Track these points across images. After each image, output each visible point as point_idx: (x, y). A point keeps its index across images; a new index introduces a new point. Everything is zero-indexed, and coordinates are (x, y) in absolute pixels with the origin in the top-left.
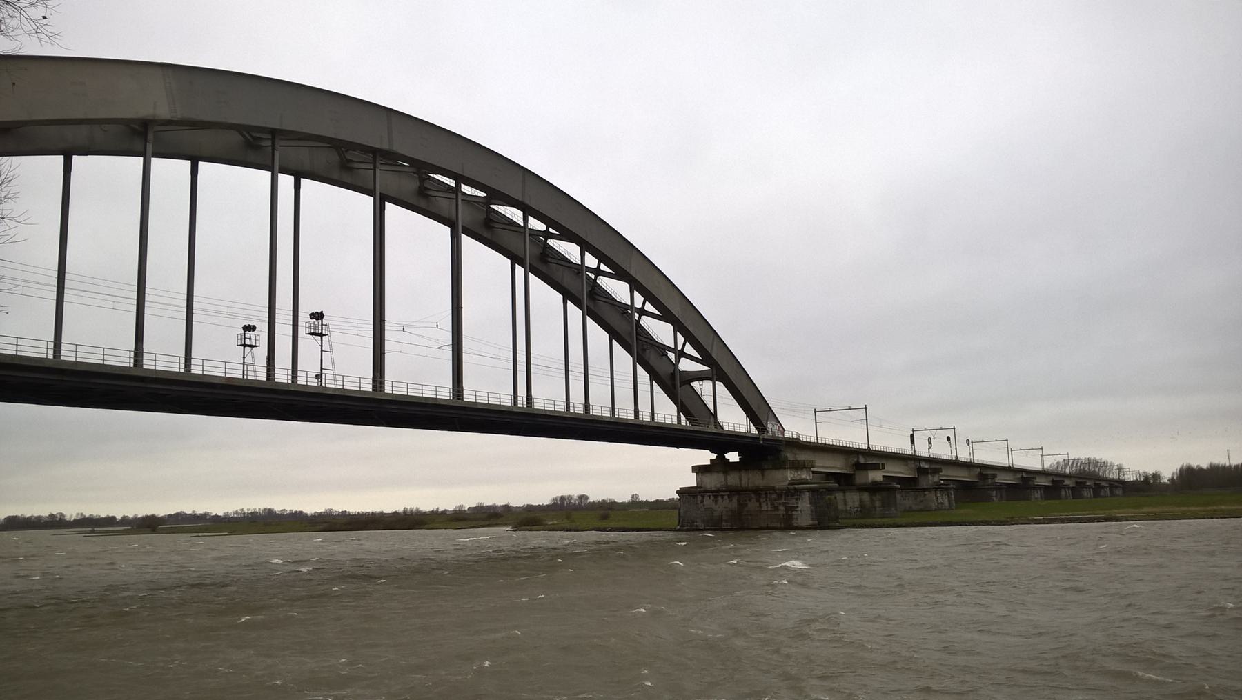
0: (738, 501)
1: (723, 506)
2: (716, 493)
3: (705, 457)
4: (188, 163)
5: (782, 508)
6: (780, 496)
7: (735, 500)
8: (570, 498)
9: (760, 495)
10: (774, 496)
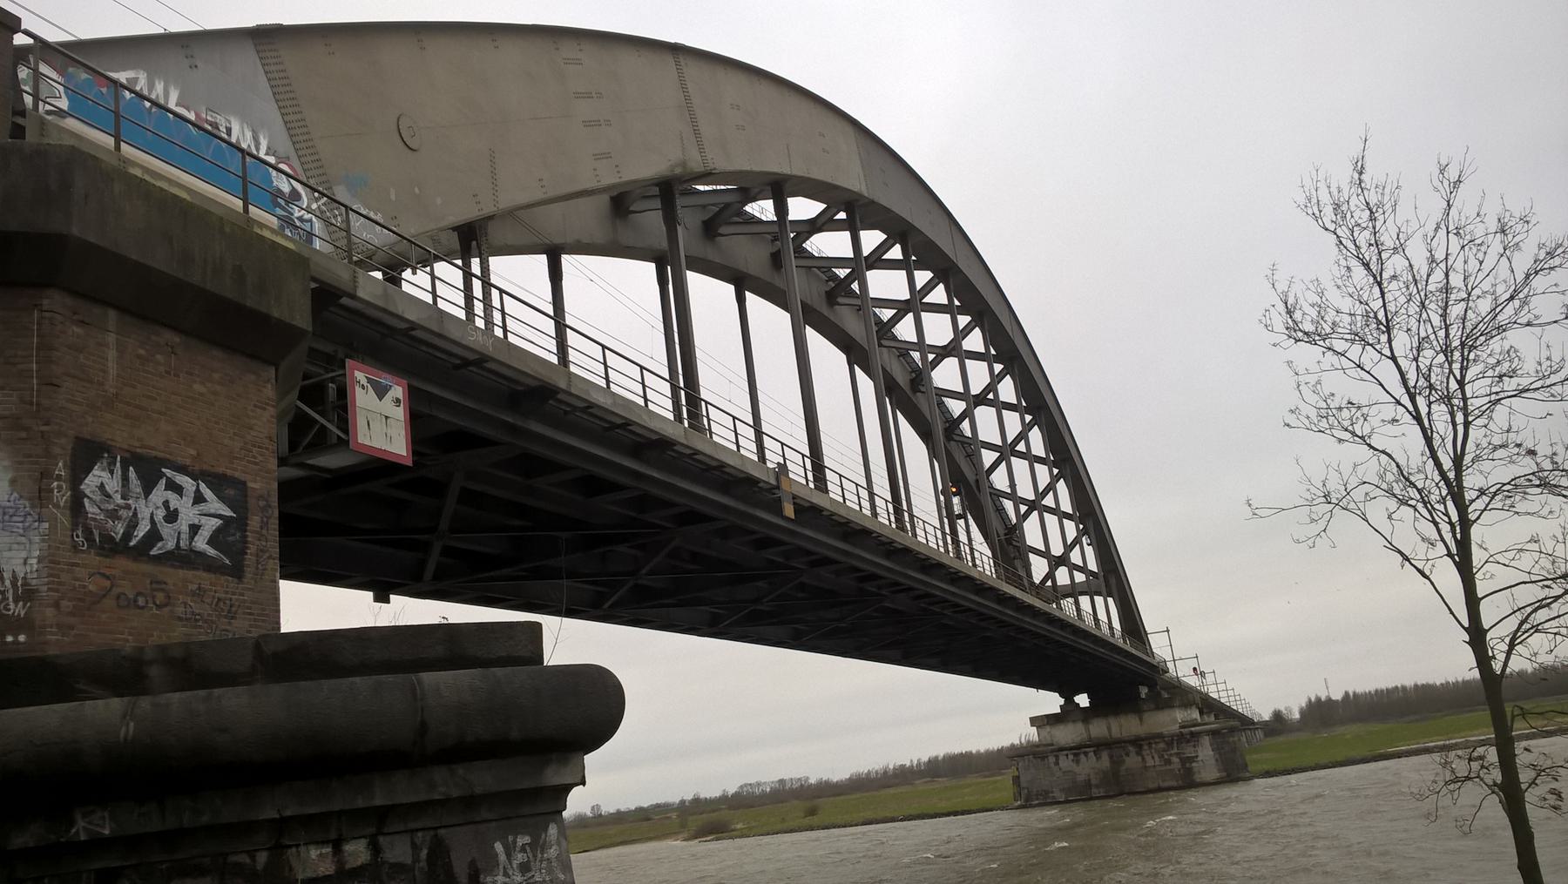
0: (1111, 757)
1: (1090, 767)
2: (1077, 750)
3: (1051, 702)
5: (1175, 760)
6: (1170, 744)
7: (1105, 756)
9: (1140, 747)
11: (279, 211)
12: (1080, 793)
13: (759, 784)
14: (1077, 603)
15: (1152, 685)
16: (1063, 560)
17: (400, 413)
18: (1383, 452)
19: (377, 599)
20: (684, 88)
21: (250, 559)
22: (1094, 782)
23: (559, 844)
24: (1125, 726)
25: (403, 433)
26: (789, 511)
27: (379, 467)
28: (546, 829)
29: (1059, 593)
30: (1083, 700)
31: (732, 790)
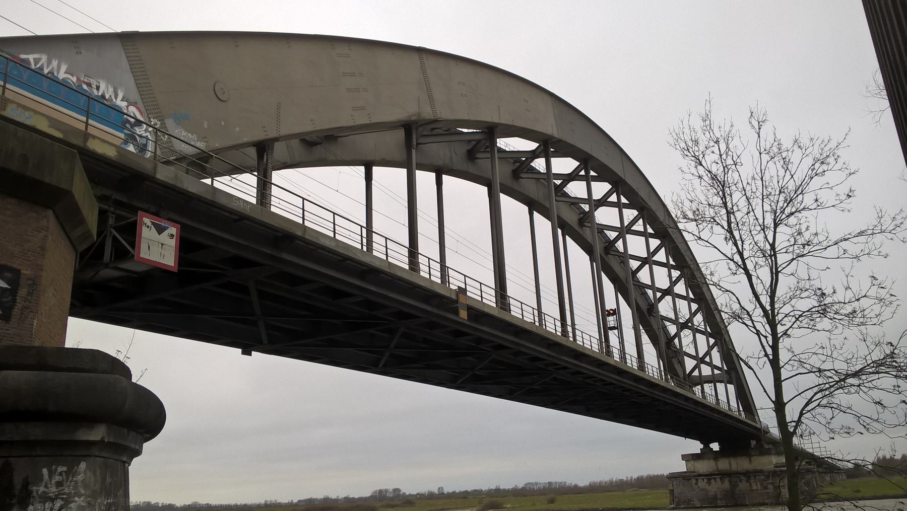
0: (730, 482)
1: (716, 487)
2: (709, 476)
3: (695, 446)
4: (362, 169)
5: (771, 487)
6: (768, 477)
8: (386, 491)
11: (126, 131)
13: (536, 484)
15: (759, 440)
16: (702, 361)
17: (173, 243)
19: (243, 353)
20: (424, 72)
21: (16, 311)
22: (719, 496)
24: (740, 464)
26: (463, 314)
27: (157, 272)
29: (702, 380)
30: (715, 446)
31: (520, 486)
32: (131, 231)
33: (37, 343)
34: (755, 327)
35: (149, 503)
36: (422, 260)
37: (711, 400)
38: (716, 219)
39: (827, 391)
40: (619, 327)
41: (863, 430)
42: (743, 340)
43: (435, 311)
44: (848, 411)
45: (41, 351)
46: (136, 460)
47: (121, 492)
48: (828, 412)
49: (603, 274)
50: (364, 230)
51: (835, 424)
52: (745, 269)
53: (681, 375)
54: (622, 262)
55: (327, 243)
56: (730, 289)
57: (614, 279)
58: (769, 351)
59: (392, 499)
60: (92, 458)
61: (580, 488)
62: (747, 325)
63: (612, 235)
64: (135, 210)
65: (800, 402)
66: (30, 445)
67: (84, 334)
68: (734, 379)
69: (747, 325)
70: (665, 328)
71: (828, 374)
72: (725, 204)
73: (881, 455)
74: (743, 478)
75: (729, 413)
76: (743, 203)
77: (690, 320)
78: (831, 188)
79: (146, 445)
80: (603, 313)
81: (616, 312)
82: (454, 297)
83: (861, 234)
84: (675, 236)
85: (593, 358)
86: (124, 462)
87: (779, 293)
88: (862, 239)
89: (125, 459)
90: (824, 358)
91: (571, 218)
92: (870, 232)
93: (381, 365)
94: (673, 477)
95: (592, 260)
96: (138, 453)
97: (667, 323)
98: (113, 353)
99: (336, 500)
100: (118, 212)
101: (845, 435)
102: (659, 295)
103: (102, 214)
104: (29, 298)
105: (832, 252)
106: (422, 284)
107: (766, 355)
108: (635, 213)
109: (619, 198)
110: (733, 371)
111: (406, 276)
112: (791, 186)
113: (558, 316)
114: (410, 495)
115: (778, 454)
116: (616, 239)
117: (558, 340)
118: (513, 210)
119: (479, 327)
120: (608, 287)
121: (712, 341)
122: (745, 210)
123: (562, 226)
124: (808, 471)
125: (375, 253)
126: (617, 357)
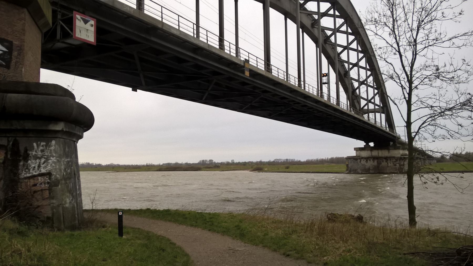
0: (377, 162)
1: (370, 164)
2: (367, 159)
3: (361, 144)
5: (398, 165)
6: (397, 160)
7: (376, 161)
8: (206, 161)
9: (387, 160)
10: (394, 160)
12: (366, 171)
13: (280, 160)
14: (368, 115)
15: (394, 142)
16: (370, 101)
17: (93, 29)
18: (390, 64)
19: (133, 90)
23: (55, 146)
24: (384, 153)
25: (93, 35)
26: (247, 74)
27: (85, 45)
28: (51, 141)
29: (368, 111)
30: (372, 144)
31: (272, 160)
32: (70, 22)
33: (25, 80)
34: (401, 83)
35: (89, 163)
36: (226, 43)
37: (372, 121)
38: (387, 23)
39: (433, 117)
40: (328, 83)
41: (450, 137)
42: (393, 89)
43: (232, 71)
44: (444, 128)
45: (27, 84)
46: (80, 141)
47: (74, 156)
48: (432, 128)
49: (323, 56)
50: (195, 26)
51: (437, 134)
52: (399, 52)
53: (358, 108)
54: (333, 48)
55: (175, 32)
56: (388, 63)
57: (328, 57)
58: (407, 96)
59: (209, 164)
60: (58, 139)
61: (302, 162)
62: (397, 82)
63: (329, 33)
64: (71, 11)
65: (420, 122)
66: (26, 132)
67: (48, 76)
68: (385, 112)
69: (397, 82)
70: (352, 84)
71: (436, 109)
72: (393, 15)
73: (455, 152)
74: (384, 160)
75: (381, 128)
76: (402, 15)
77: (366, 80)
78: (452, 8)
79: (85, 134)
80: (321, 75)
81: (327, 75)
82: (242, 64)
83: (465, 34)
84: (362, 33)
85: (314, 98)
86: (75, 141)
87: (414, 67)
88: (463, 37)
89: (74, 140)
90: (435, 100)
91: (308, 23)
92: (470, 34)
93: (204, 99)
94: (349, 158)
95: (317, 47)
96: (81, 137)
97: (353, 81)
98: (65, 87)
99: (181, 164)
100: (62, 11)
101: (442, 139)
102: (351, 66)
103: (54, 12)
104: (19, 57)
105: (447, 44)
106: (226, 56)
107: (405, 98)
108: (343, 20)
109: (334, 12)
110: (385, 108)
111: (217, 52)
112: (429, 7)
113: (297, 76)
114: (218, 163)
115: (404, 149)
116: (331, 35)
117: (296, 89)
118: (276, 17)
119: (255, 81)
120: (325, 61)
121: (376, 91)
122: (403, 19)
123: (302, 27)
124: (417, 158)
125: (201, 39)
126: (326, 98)
